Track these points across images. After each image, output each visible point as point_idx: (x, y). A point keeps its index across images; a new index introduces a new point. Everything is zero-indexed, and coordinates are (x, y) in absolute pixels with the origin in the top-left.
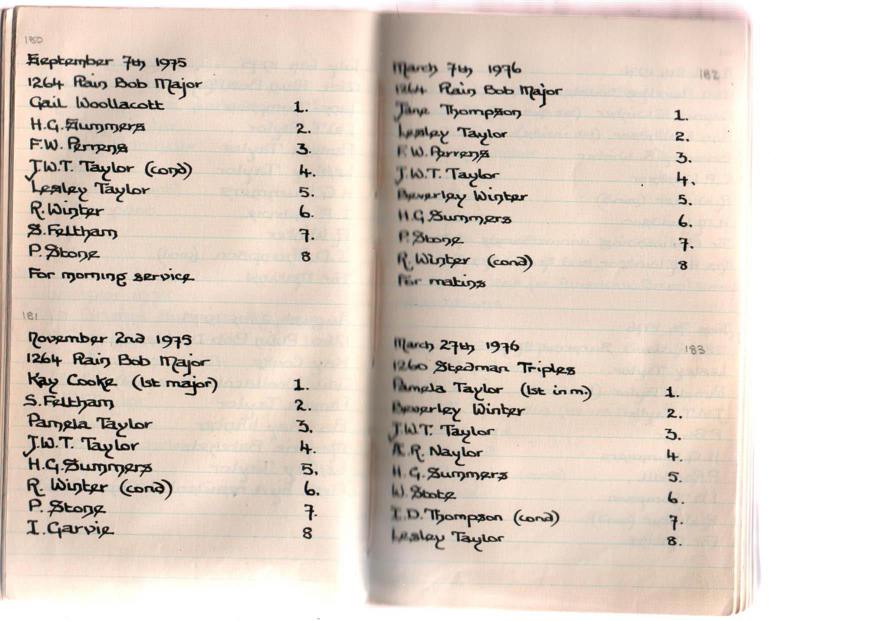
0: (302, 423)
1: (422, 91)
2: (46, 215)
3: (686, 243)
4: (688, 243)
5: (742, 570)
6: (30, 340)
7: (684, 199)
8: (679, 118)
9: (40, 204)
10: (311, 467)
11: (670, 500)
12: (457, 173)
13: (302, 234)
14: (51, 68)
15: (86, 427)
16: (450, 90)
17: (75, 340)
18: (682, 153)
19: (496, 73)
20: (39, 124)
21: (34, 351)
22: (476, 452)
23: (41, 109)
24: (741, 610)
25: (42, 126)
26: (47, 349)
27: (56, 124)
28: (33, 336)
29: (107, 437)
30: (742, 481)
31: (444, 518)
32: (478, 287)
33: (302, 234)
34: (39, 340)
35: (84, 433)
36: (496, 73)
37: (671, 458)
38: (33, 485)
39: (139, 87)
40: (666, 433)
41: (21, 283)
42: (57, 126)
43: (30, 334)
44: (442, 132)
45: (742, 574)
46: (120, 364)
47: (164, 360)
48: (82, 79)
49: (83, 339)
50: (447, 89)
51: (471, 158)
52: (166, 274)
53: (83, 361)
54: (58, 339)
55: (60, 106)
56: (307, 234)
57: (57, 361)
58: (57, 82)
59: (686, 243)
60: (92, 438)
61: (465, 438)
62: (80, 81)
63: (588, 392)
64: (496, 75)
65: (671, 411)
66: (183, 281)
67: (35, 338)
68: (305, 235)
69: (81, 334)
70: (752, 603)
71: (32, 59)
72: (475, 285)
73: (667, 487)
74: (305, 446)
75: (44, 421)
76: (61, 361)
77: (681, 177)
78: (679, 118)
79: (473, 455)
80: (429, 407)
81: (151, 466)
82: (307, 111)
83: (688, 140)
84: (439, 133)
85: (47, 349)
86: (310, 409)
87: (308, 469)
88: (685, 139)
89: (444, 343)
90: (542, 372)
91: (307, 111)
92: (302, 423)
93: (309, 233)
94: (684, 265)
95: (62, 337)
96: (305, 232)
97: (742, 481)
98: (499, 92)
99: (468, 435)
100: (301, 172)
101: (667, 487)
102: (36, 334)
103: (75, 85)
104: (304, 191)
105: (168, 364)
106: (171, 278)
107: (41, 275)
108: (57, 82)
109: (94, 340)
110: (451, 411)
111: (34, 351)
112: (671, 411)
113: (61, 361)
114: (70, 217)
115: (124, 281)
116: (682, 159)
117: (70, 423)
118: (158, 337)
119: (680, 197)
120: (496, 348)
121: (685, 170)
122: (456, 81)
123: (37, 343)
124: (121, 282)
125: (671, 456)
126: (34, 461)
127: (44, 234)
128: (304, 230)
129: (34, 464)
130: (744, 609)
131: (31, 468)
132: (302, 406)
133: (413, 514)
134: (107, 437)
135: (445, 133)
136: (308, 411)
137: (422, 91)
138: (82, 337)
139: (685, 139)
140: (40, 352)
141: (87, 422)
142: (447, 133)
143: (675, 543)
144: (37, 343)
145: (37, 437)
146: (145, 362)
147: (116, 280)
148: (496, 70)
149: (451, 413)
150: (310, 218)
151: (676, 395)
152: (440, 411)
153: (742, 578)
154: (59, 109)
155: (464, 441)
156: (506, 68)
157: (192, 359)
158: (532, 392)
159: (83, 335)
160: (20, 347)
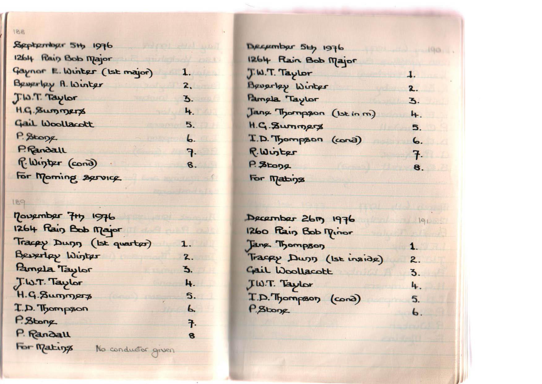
0: (186, 268)
1: (32, 60)
2: (28, 166)
3: (418, 154)
4: (192, 284)
5: (461, 357)
6: (15, 217)
7: (190, 124)
8: (185, 74)
9: (25, 159)
10: (191, 295)
11: (188, 140)
12: (293, 99)
13: (189, 152)
14: (28, 49)
15: (52, 271)
16: (282, 231)
17: (44, 216)
18: (187, 96)
19: (97, 48)
20: (23, 295)
21: (18, 224)
22: (78, 282)
23: (18, 74)
24: (460, 381)
25: (24, 295)
26: (27, 222)
27: (34, 294)
28: (17, 215)
29: (65, 277)
30: (459, 302)
31: (49, 309)
32: (299, 182)
33: (189, 152)
34: (21, 217)
35: (51, 275)
36: (97, 48)
37: (414, 287)
38: (20, 162)
39: (317, 234)
40: (183, 269)
41: (12, 182)
42: (35, 295)
43: (15, 214)
44: (50, 84)
45: (461, 360)
46: (71, 231)
47: (95, 230)
48: (46, 56)
49: (281, 218)
50: (45, 58)
51: (335, 297)
52: (104, 177)
53: (50, 229)
54: (34, 217)
55: (33, 125)
56: (192, 152)
57: (34, 230)
58: (32, 228)
59: (418, 154)
60: (55, 278)
61: (73, 274)
62: (48, 228)
63: (149, 243)
64: (97, 49)
65: (413, 258)
66: (113, 180)
67: (17, 216)
68: (191, 152)
69: (281, 216)
70: (467, 378)
71: (18, 45)
72: (297, 181)
73: (412, 305)
74: (414, 285)
75: (25, 268)
76: (36, 230)
77: (188, 110)
78: (185, 74)
79: (307, 286)
80: (40, 254)
81: (91, 295)
82: (417, 91)
83: (191, 88)
84: (49, 84)
85: (27, 222)
86: (419, 262)
87: (190, 295)
88: (189, 87)
89: (305, 217)
90: (301, 115)
91: (417, 91)
92: (186, 268)
93: (193, 151)
94: (417, 167)
95: (36, 215)
96: (191, 150)
97: (459, 302)
98: (74, 59)
99: (76, 271)
100: (412, 115)
101: (412, 305)
102: (19, 213)
103: (43, 59)
104: (188, 124)
105: (98, 231)
106: (106, 179)
107: (23, 177)
108: (32, 228)
109: (53, 217)
110: (54, 256)
111: (18, 224)
112: (186, 255)
113: (36, 230)
114: (49, 142)
115: (75, 180)
116: (187, 100)
117: (41, 268)
118: (93, 214)
119: (187, 123)
120: (330, 49)
121: (415, 108)
122: (286, 225)
123: (20, 219)
124: (73, 181)
125: (188, 284)
126: (20, 293)
127: (26, 297)
128: (190, 149)
129: (21, 295)
130: (462, 381)
131: (17, 111)
132: (188, 257)
133: (263, 139)
134: (65, 277)
135: (52, 84)
136: (191, 260)
137: (32, 60)
138: (48, 214)
139: (189, 87)
140: (22, 225)
141: (258, 268)
142: (54, 84)
143: (192, 167)
144: (20, 219)
145: (254, 281)
146: (86, 231)
147: (70, 179)
148: (97, 46)
149: (54, 257)
150: (192, 142)
151: (416, 249)
152: (46, 257)
153: (461, 363)
154: (33, 127)
155: (72, 275)
156: (334, 47)
157: (112, 228)
158: (100, 244)
159: (282, 216)
160: (11, 222)
